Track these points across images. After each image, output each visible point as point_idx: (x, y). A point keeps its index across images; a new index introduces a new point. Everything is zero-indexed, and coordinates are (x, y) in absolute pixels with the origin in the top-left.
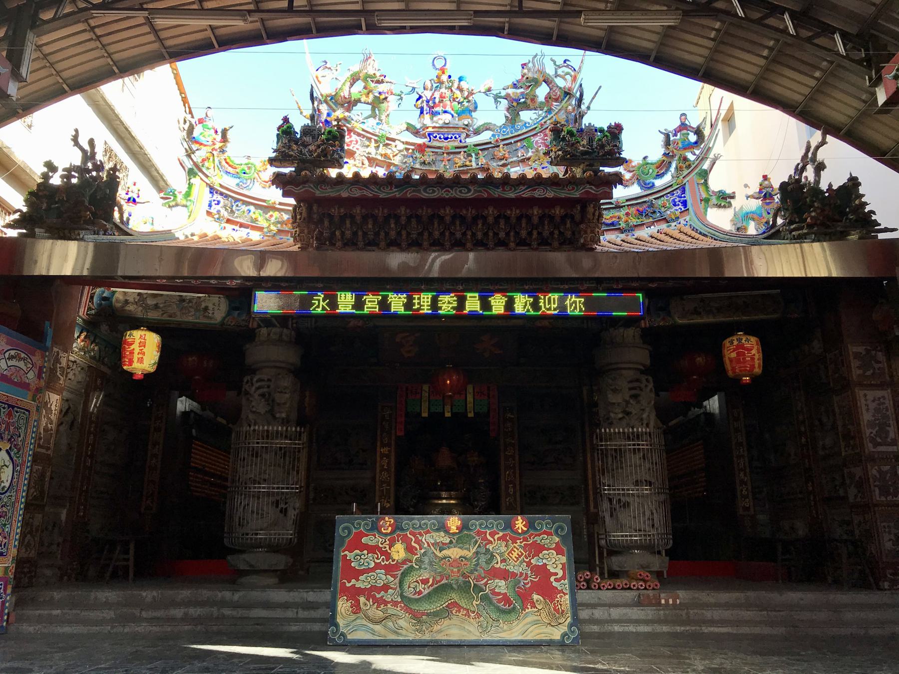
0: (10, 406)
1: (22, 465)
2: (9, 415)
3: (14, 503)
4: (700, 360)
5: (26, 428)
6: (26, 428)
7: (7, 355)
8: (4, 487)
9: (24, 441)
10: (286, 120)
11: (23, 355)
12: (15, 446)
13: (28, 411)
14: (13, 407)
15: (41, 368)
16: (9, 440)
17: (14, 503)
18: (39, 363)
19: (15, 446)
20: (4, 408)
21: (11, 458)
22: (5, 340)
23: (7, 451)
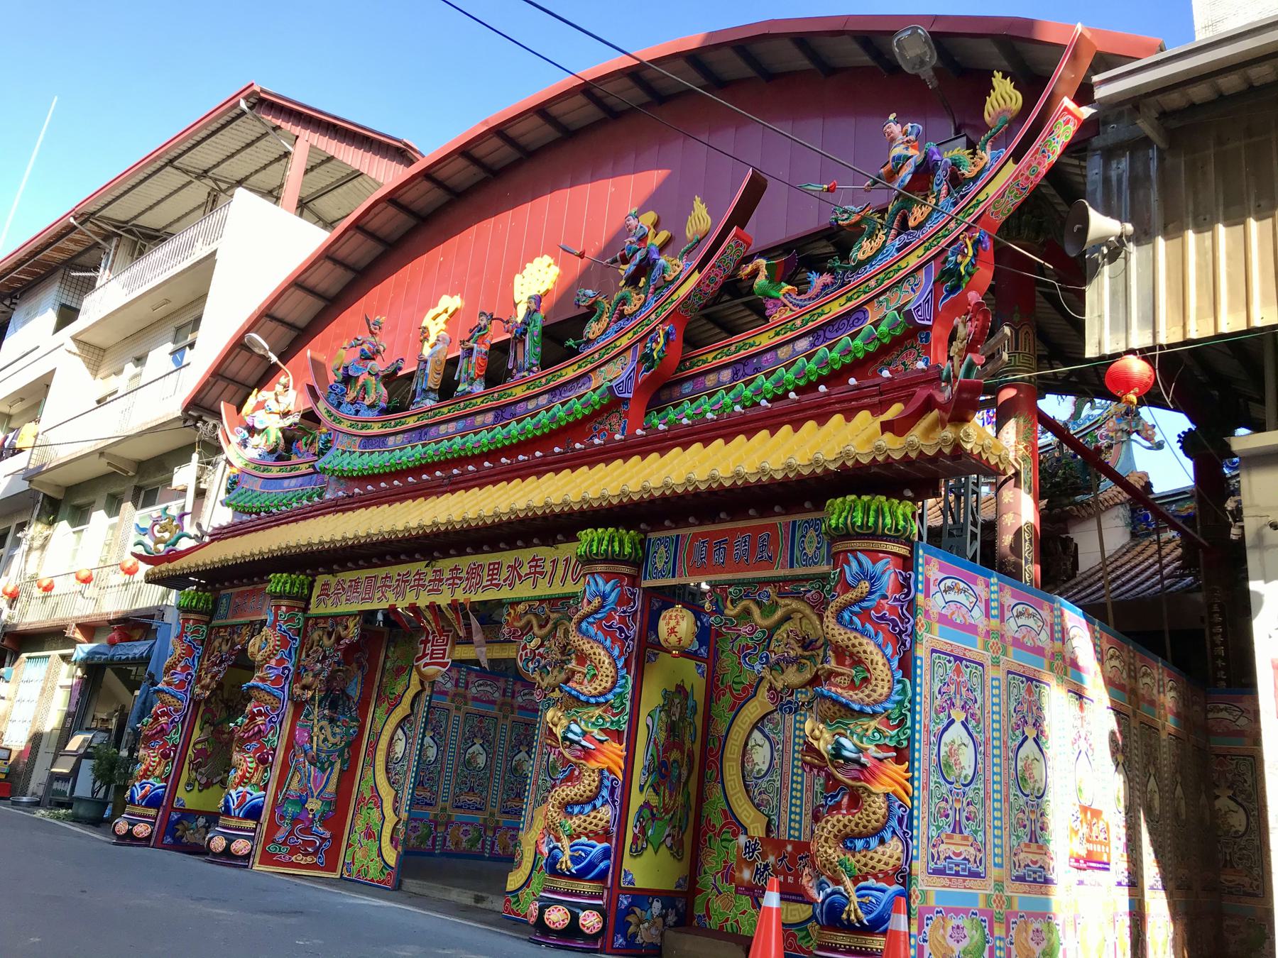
0: (957, 658)
1: (414, 737)
2: (958, 671)
3: (405, 773)
4: (471, 468)
5: (983, 691)
6: (983, 691)
7: (942, 586)
8: (760, 770)
9: (983, 707)
10: (53, 371)
11: (962, 585)
12: (972, 715)
13: (982, 665)
14: (961, 660)
15: (987, 602)
16: (963, 707)
17: (779, 791)
18: (984, 595)
19: (972, 715)
20: (949, 662)
21: (970, 734)
22: (937, 566)
23: (963, 723)
